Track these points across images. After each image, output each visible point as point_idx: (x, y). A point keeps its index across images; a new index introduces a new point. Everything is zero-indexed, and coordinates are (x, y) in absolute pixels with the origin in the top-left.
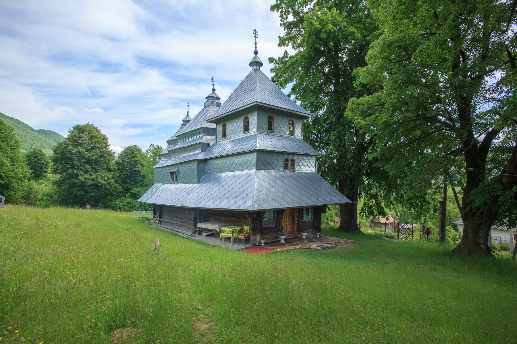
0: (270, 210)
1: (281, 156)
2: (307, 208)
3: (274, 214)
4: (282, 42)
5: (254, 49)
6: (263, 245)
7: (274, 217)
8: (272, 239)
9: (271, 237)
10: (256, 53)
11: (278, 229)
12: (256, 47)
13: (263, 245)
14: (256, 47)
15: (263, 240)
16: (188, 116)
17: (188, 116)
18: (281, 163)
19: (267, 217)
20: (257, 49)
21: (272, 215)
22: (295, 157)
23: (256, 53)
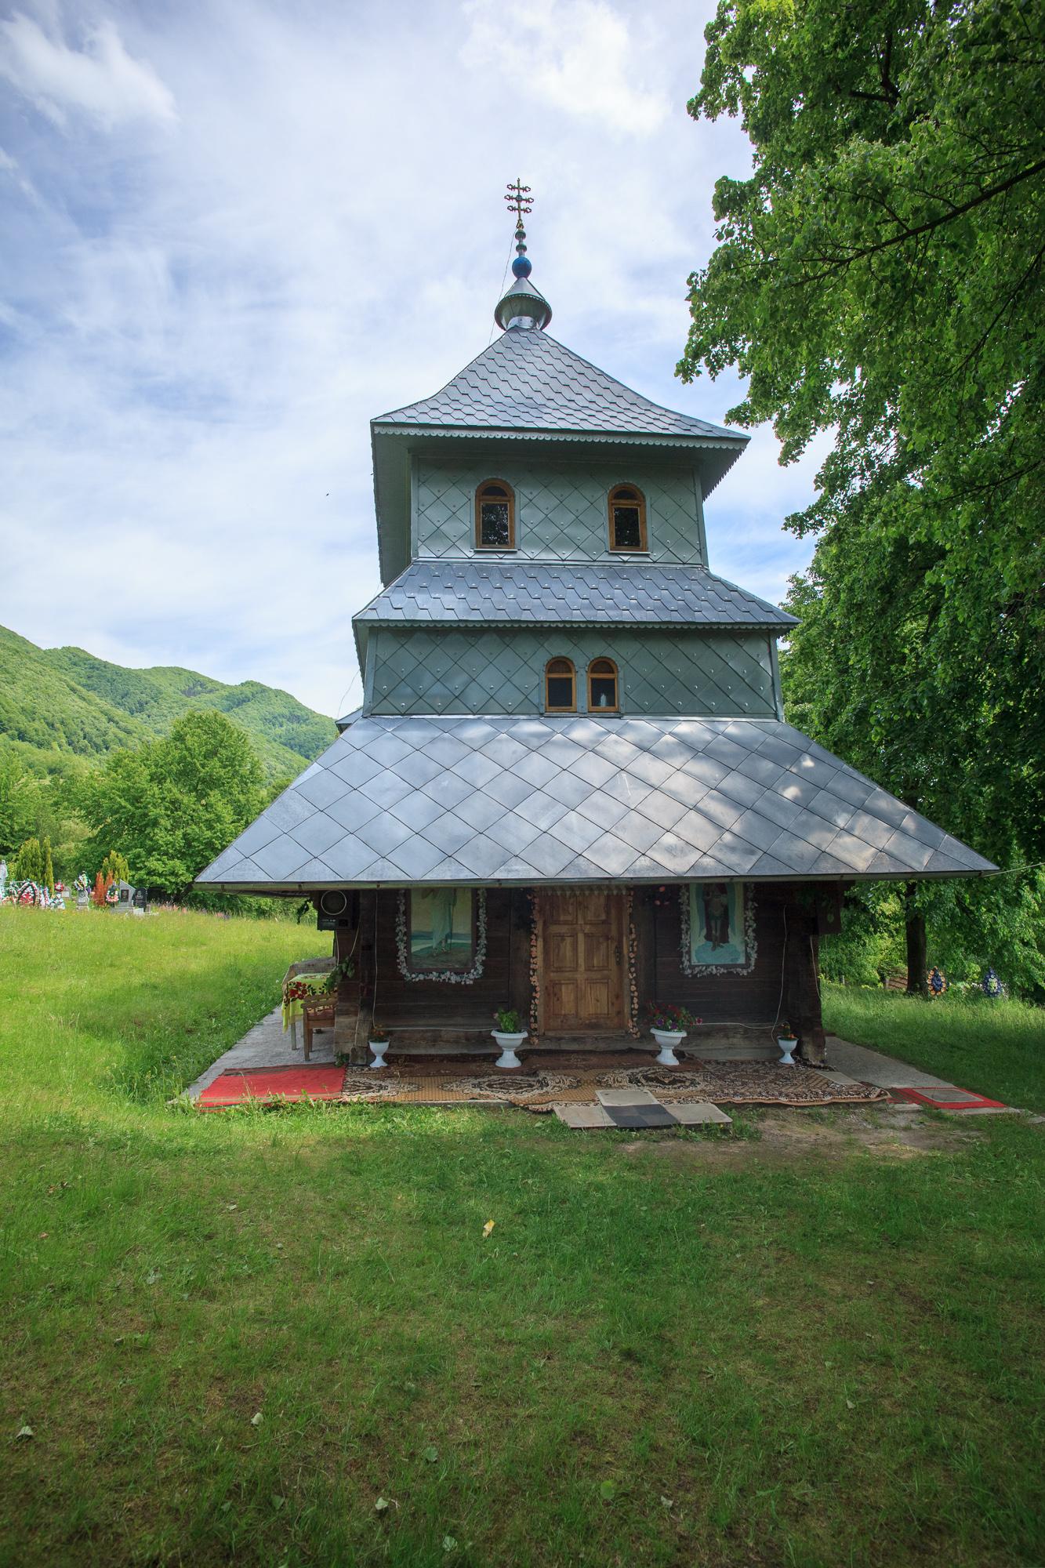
0: (444, 893)
1: (526, 647)
2: (714, 892)
3: (476, 917)
4: (717, 219)
5: (516, 255)
6: (378, 1063)
7: (476, 936)
8: (456, 1042)
9: (449, 1031)
10: (522, 269)
11: (501, 991)
12: (521, 248)
13: (378, 1063)
14: (521, 248)
15: (380, 1040)
16: (524, 309)
17: (524, 309)
18: (534, 681)
19: (428, 936)
20: (527, 255)
21: (463, 926)
22: (620, 653)
23: (522, 269)
